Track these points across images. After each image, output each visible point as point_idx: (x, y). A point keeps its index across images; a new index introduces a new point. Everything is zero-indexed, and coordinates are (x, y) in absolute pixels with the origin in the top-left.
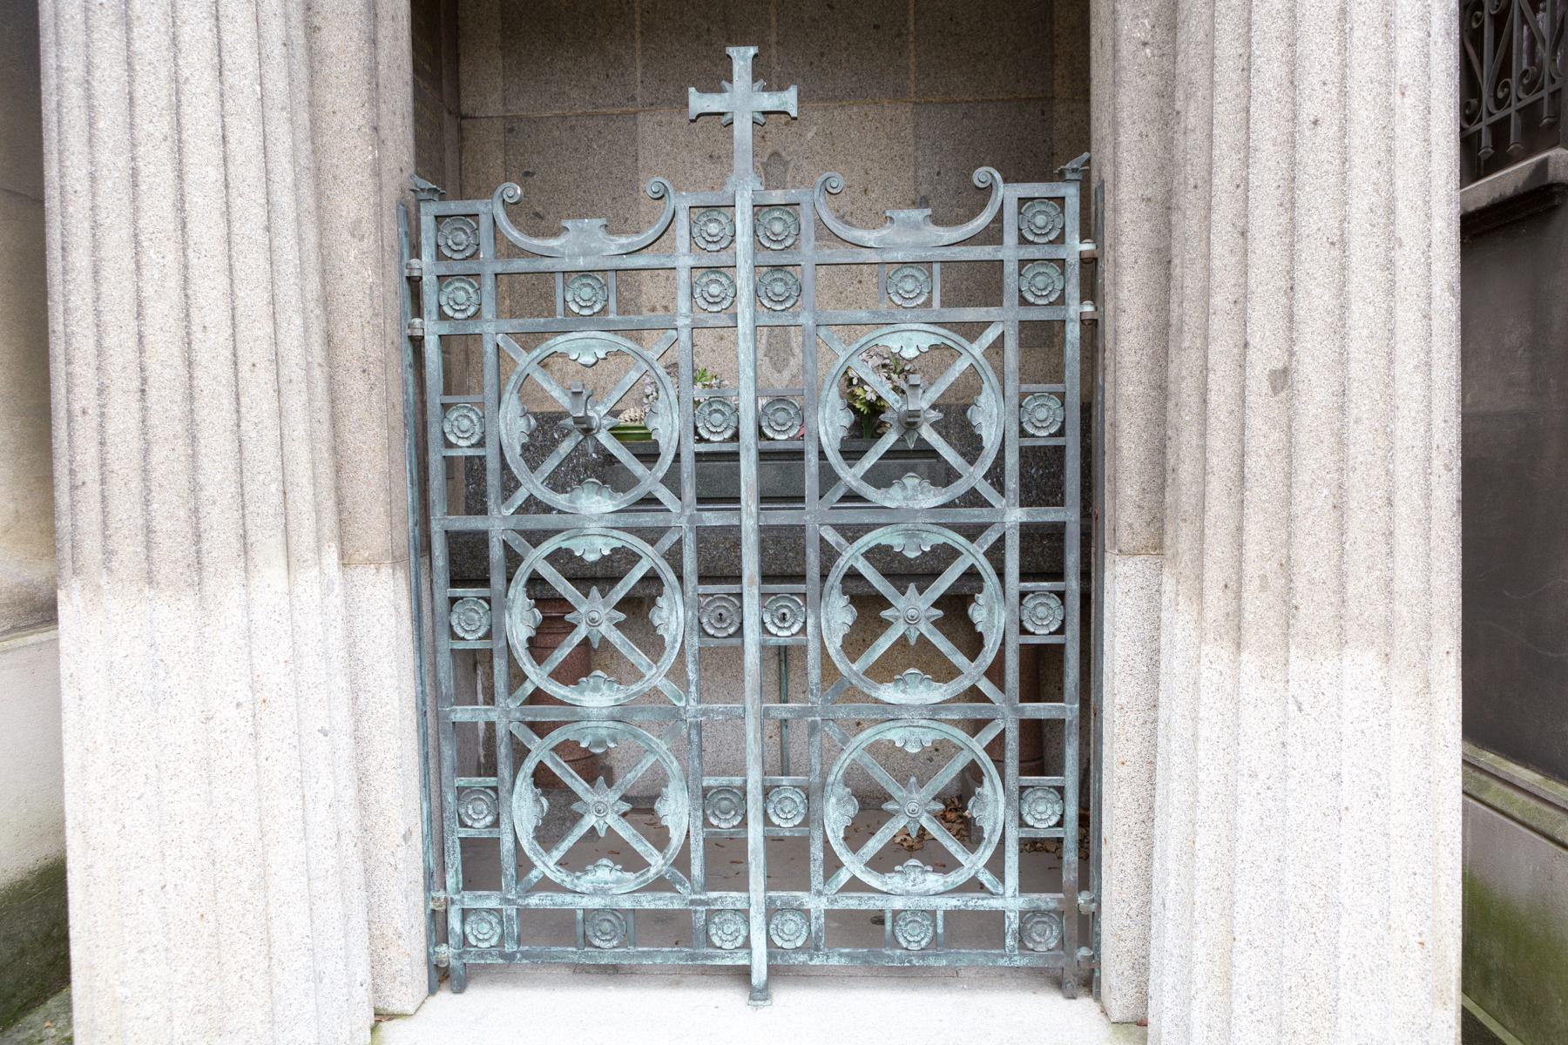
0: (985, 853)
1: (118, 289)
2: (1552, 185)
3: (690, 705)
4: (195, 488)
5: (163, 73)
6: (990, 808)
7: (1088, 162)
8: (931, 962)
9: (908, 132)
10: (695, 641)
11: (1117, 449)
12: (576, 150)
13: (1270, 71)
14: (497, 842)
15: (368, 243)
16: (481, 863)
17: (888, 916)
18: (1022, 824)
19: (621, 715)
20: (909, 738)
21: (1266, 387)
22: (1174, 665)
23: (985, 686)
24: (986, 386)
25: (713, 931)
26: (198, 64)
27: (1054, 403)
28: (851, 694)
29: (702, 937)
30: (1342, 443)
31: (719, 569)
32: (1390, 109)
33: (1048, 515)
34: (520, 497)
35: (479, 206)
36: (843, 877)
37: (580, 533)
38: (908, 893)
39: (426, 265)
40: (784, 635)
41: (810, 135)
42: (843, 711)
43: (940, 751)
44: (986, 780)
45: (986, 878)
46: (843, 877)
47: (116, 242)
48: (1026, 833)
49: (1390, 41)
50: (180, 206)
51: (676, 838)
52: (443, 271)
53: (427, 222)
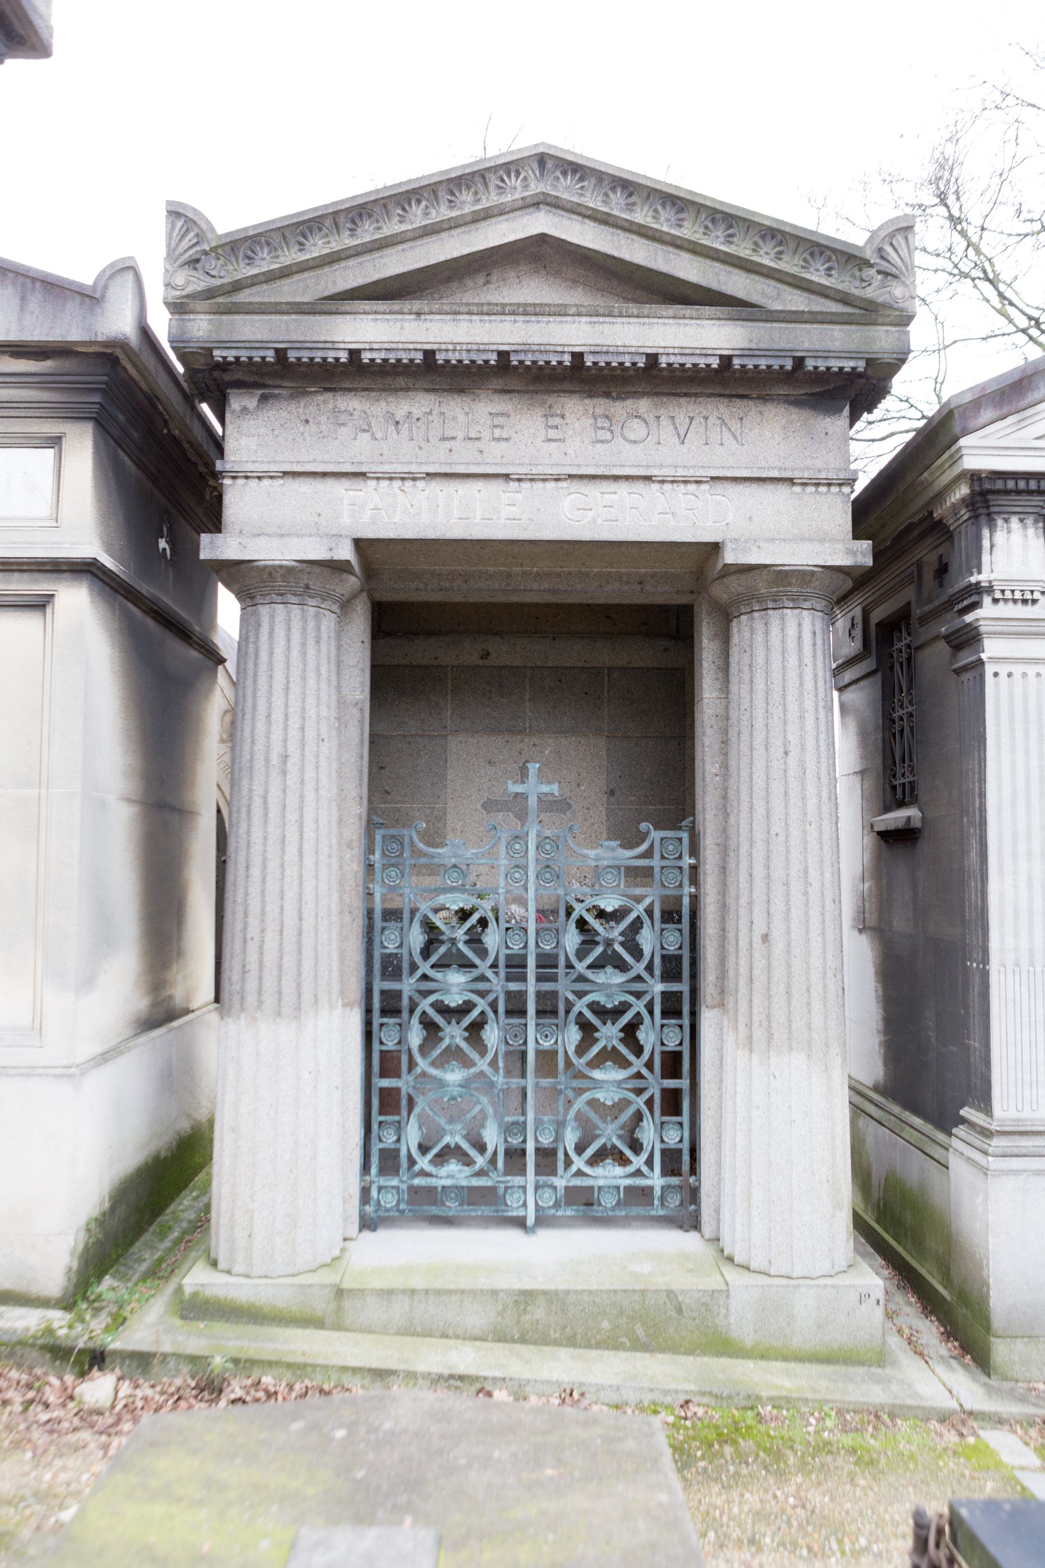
0: (644, 1156)
1: (272, 886)
2: (913, 829)
3: (500, 1079)
4: (299, 974)
5: (297, 794)
6: (646, 1133)
7: (693, 822)
8: (618, 1213)
9: (603, 753)
10: (503, 1048)
11: (705, 959)
12: (411, 755)
13: (760, 812)
14: (398, 1150)
15: (355, 851)
16: (390, 1161)
17: (596, 1189)
18: (662, 1141)
19: (465, 1084)
20: (607, 1097)
21: (760, 941)
22: (728, 1060)
23: (644, 1071)
24: (645, 925)
25: (507, 1197)
26: (309, 787)
27: (677, 934)
28: (580, 1075)
29: (502, 1200)
30: (789, 966)
31: (516, 1009)
32: (805, 832)
33: (674, 987)
34: (418, 974)
35: (405, 832)
36: (574, 1169)
37: (447, 992)
38: (606, 1177)
39: (377, 857)
40: (546, 1044)
41: (547, 752)
42: (576, 1083)
43: (625, 1103)
44: (645, 1119)
45: (645, 1169)
46: (574, 1169)
47: (273, 866)
48: (663, 1146)
49: (805, 805)
50: (300, 851)
51: (490, 1149)
52: (385, 862)
53: (378, 838)
